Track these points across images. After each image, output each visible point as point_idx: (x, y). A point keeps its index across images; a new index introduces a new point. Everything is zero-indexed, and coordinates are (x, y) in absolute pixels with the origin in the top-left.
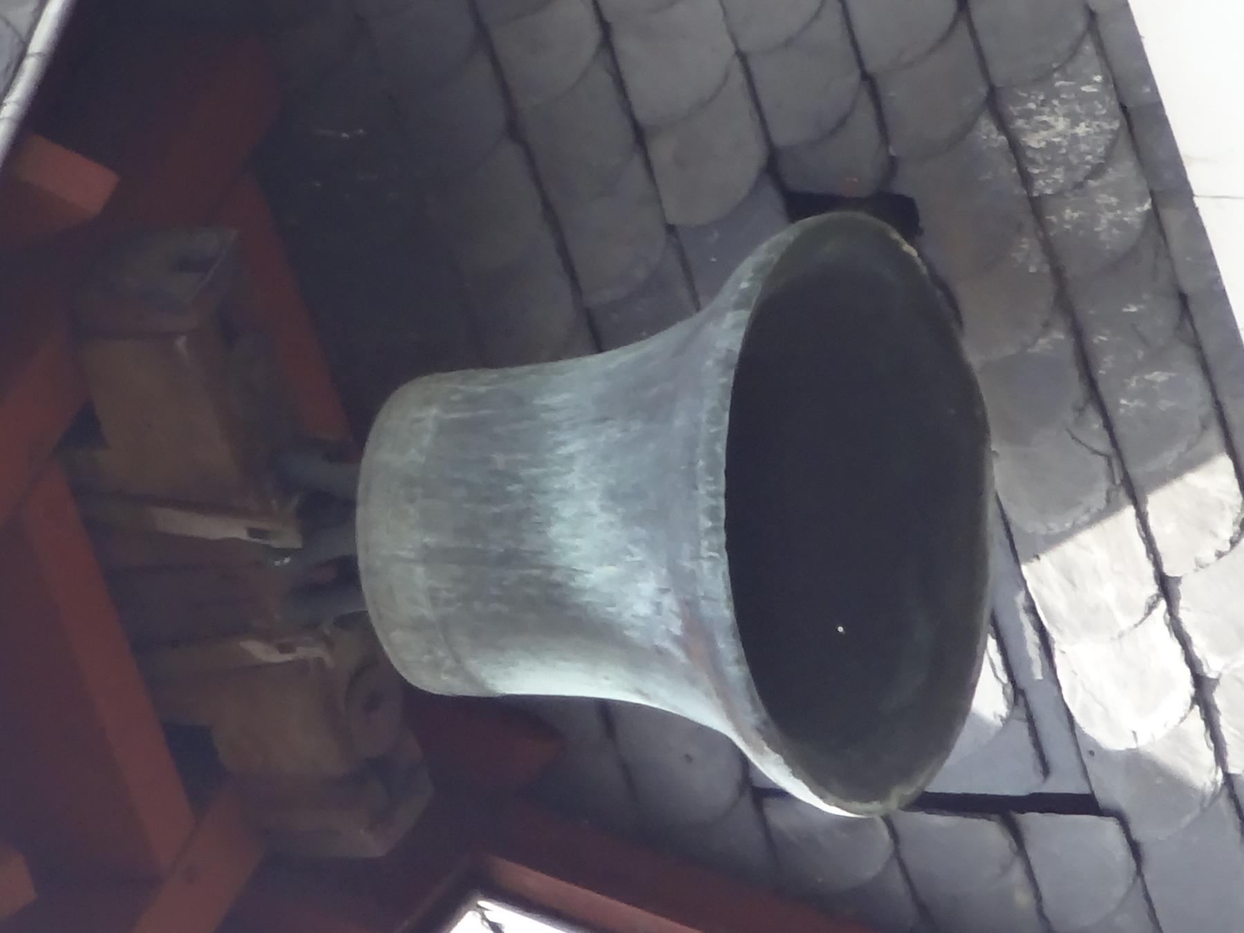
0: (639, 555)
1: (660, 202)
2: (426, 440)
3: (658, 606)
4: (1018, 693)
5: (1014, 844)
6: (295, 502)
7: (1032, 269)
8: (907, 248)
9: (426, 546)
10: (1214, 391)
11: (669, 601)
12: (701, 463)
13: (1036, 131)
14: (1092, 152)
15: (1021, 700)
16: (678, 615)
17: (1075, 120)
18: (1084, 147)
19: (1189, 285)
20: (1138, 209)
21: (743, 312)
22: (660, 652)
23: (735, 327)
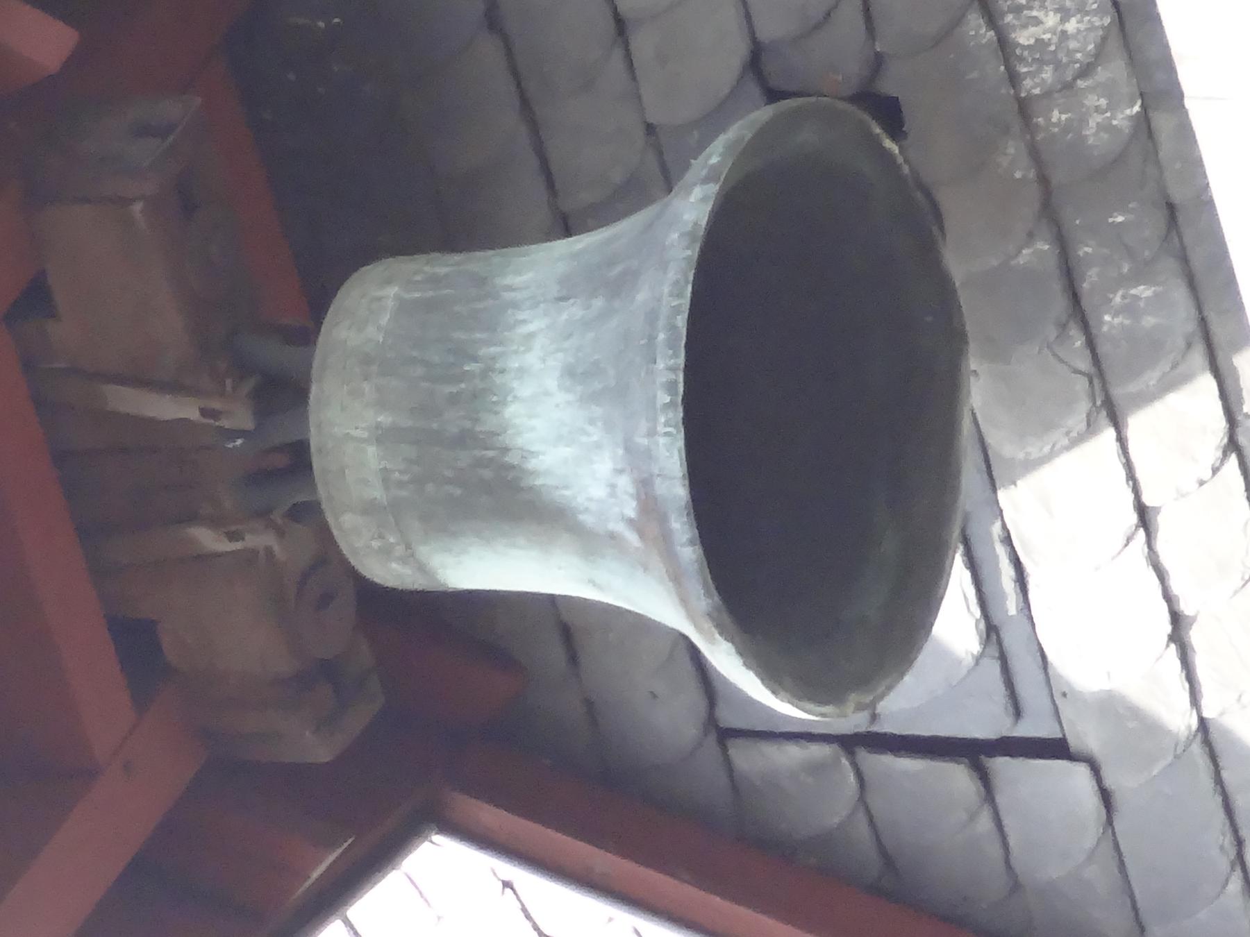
0: (596, 434)
1: (639, 97)
2: (385, 320)
3: (613, 486)
4: (991, 631)
5: (982, 789)
6: (250, 384)
7: (1018, 175)
8: (888, 144)
9: (378, 426)
10: (1199, 308)
11: (625, 483)
12: (662, 336)
13: (1025, 26)
14: (1082, 49)
15: (994, 637)
16: (632, 495)
17: (1065, 15)
18: (1073, 45)
19: (1178, 194)
20: (1128, 112)
21: (712, 185)
22: (613, 536)
23: (704, 199)
